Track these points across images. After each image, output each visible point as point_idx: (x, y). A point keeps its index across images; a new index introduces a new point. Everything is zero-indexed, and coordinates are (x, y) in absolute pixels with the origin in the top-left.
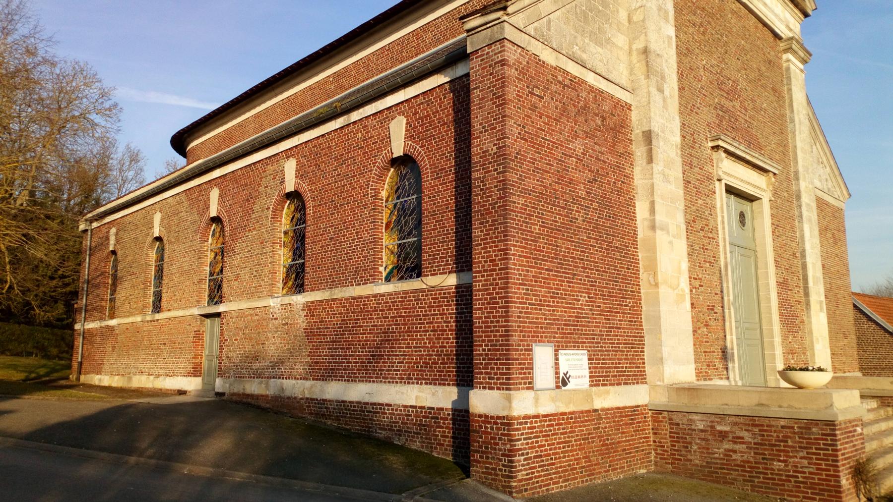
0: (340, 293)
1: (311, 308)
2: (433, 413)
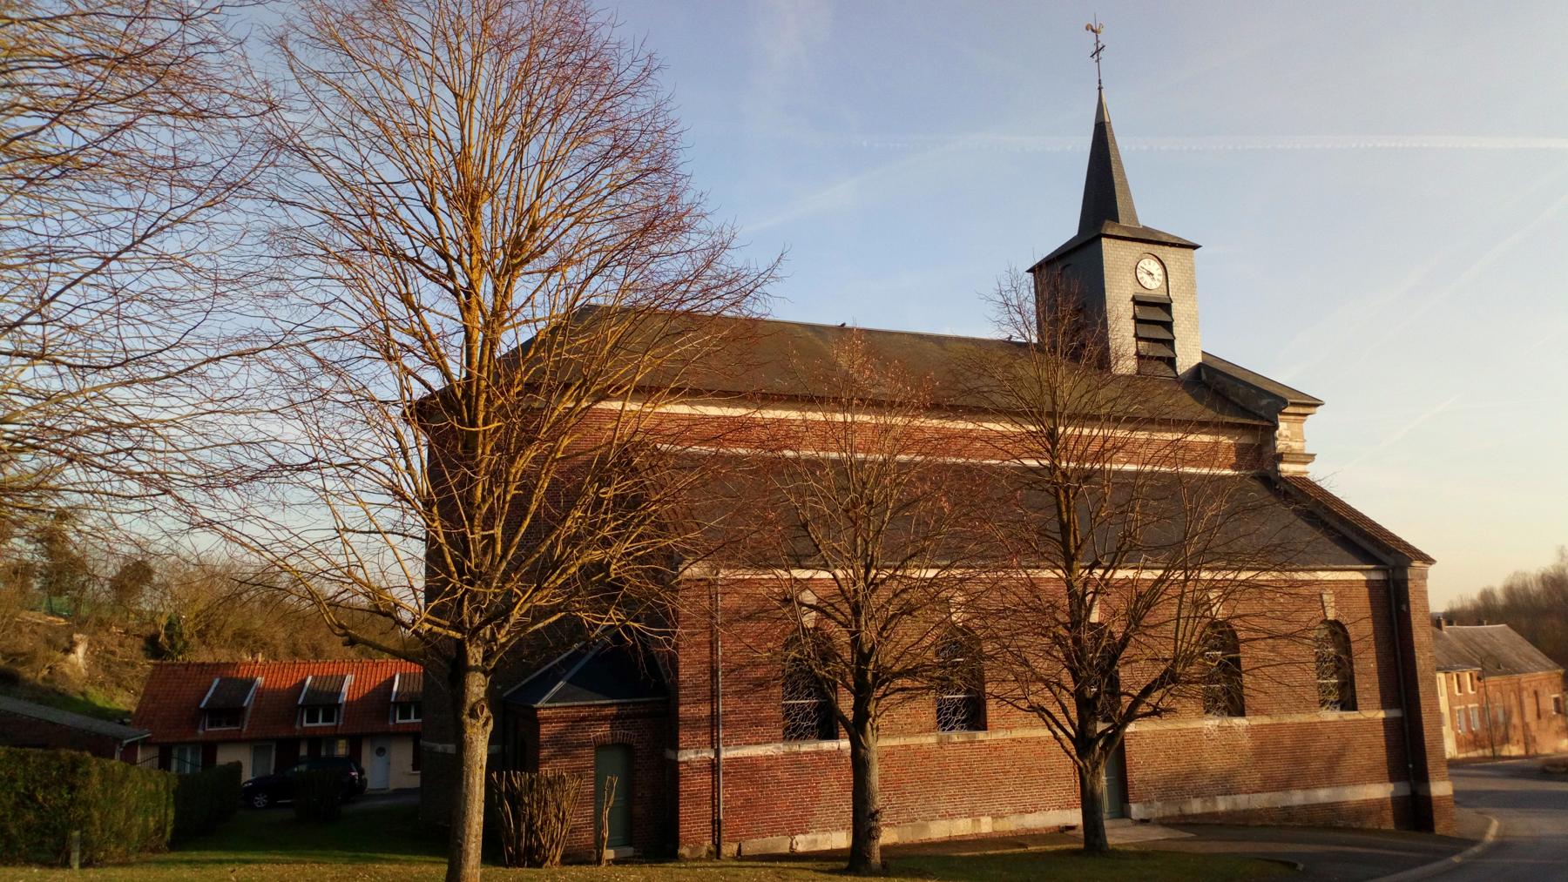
0: (1288, 720)
1: (1251, 730)
2: (1381, 802)
